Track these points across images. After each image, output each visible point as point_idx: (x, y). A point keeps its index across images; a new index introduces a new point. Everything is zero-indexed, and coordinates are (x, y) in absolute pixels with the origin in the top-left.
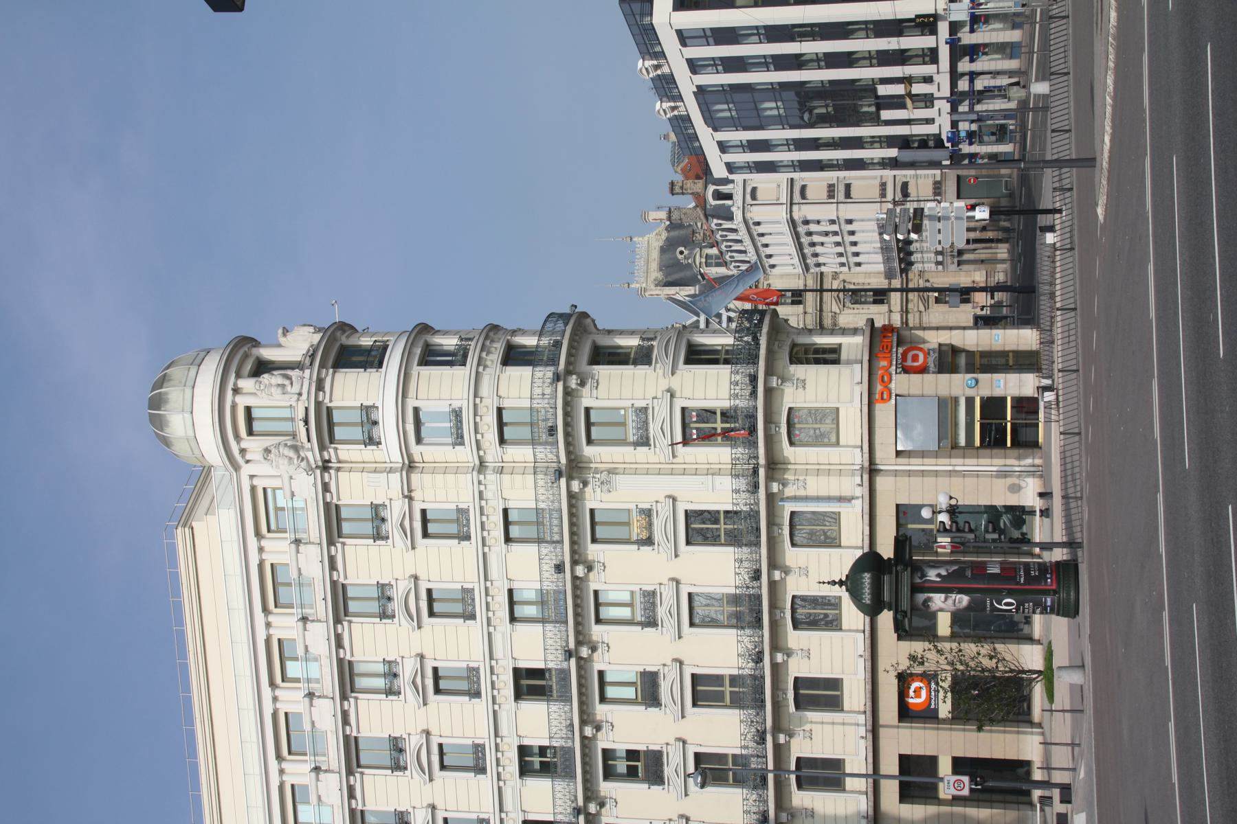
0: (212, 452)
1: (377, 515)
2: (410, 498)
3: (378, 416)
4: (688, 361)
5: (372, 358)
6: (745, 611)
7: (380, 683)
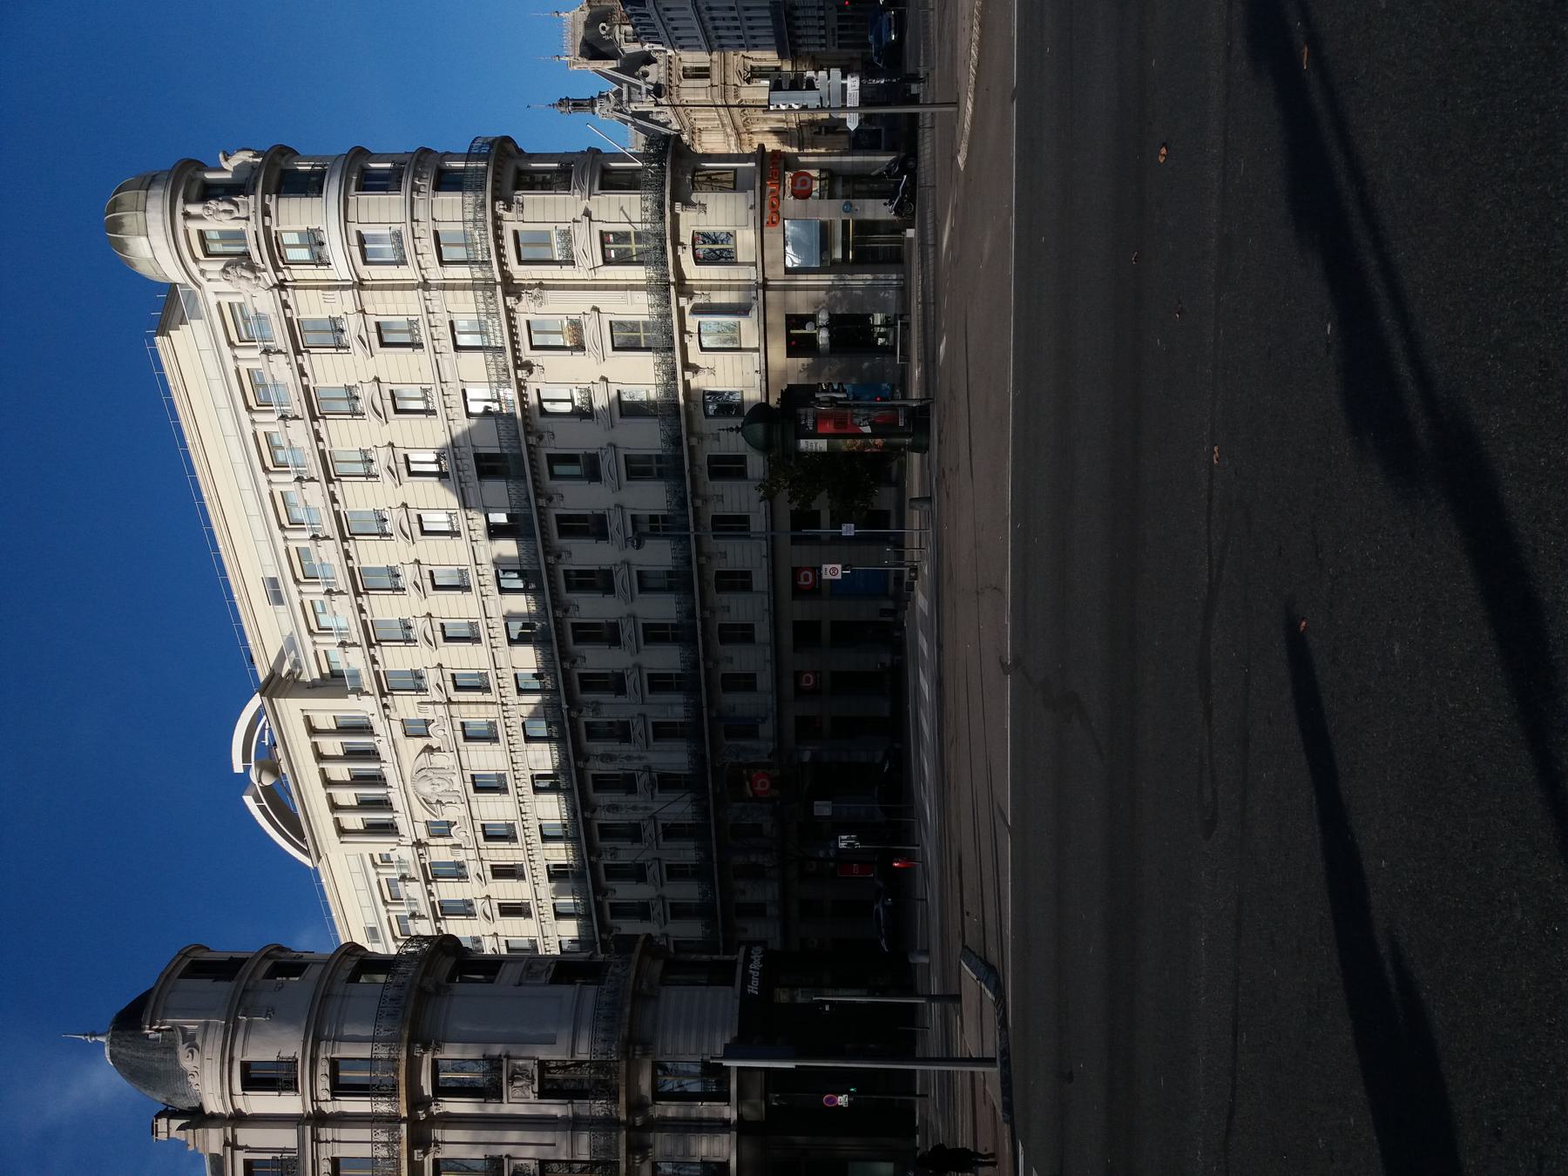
0: (174, 274)
1: (336, 327)
2: (363, 312)
3: (324, 237)
4: (602, 188)
5: (309, 185)
6: (677, 581)
7: (360, 469)
